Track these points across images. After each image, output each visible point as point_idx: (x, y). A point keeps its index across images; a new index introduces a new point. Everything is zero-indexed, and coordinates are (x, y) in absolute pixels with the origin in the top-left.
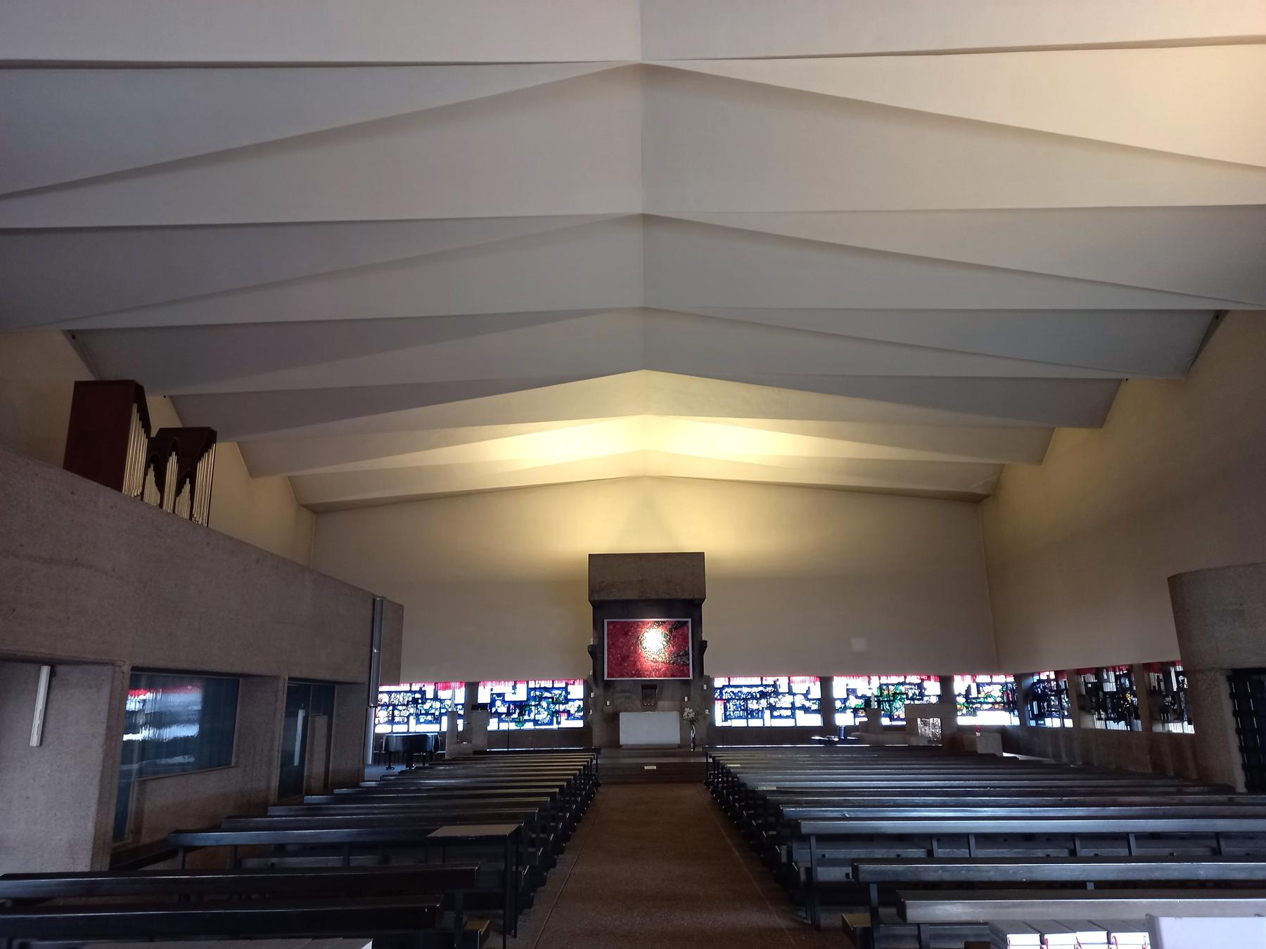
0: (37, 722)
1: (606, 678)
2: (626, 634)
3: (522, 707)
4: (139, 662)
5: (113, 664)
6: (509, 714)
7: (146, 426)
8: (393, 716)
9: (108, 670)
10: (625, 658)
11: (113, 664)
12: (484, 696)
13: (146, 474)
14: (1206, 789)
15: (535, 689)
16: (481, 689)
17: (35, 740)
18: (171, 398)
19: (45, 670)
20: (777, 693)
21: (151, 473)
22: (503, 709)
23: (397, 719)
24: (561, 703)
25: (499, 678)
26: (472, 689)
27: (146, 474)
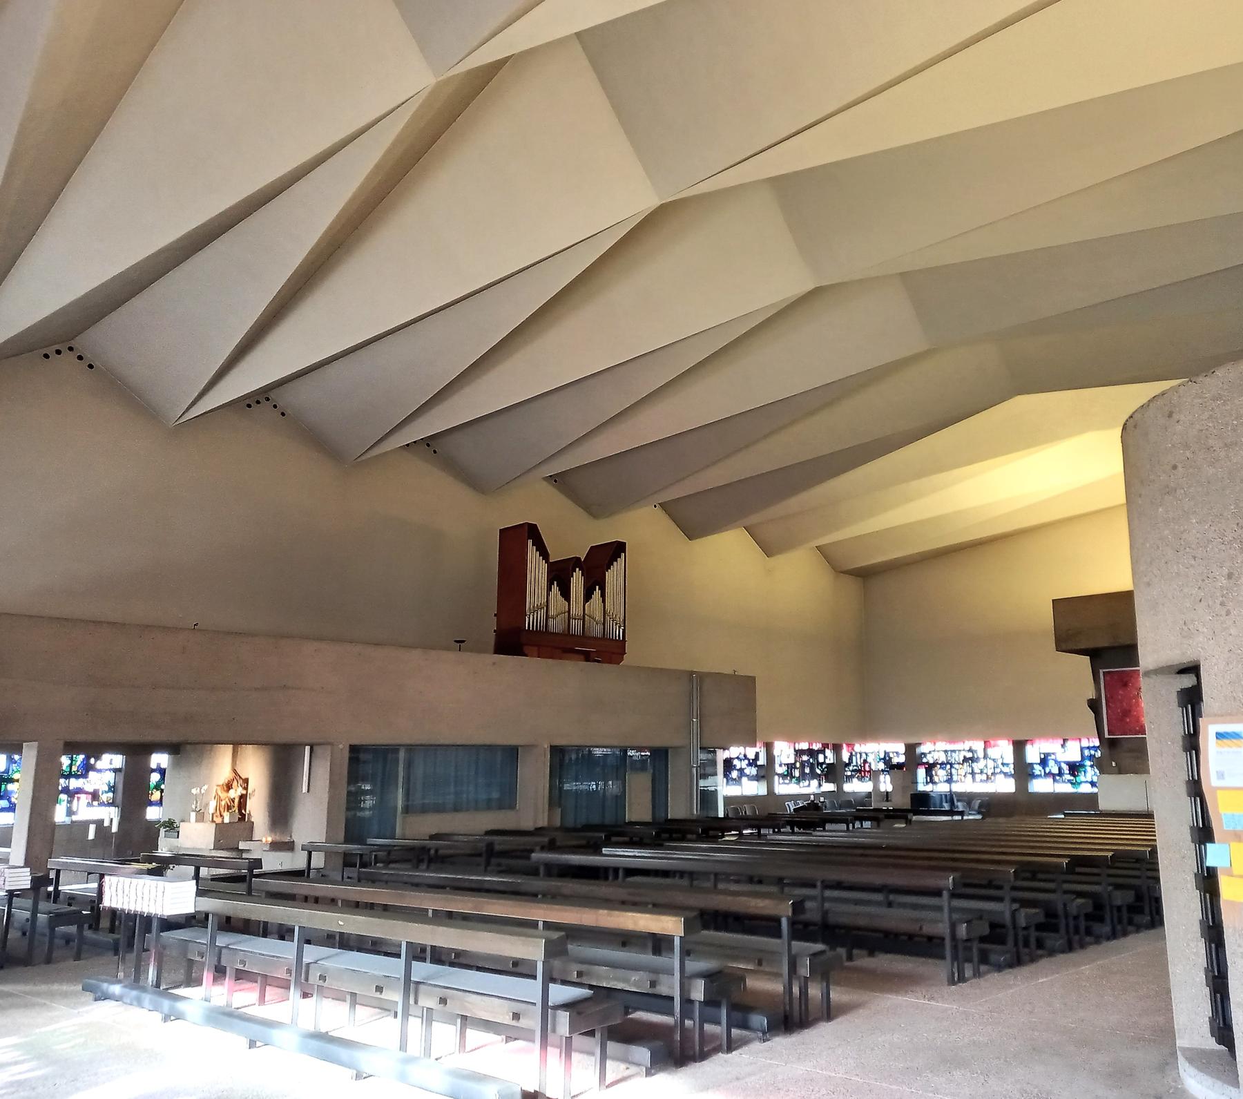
0: (305, 779)
1: (1107, 736)
2: (1125, 685)
3: (1074, 768)
4: (356, 742)
5: (331, 744)
6: (1060, 774)
7: (544, 554)
8: (951, 774)
9: (329, 747)
10: (1127, 713)
11: (331, 744)
12: (1032, 754)
13: (549, 589)
14: (456, 838)
15: (1088, 748)
16: (1029, 748)
17: (305, 789)
18: (663, 506)
19: (307, 749)
20: (973, 760)
21: (555, 588)
22: (1055, 771)
23: (955, 778)
24: (77, 777)
25: (1047, 735)
26: (1019, 747)
27: (549, 589)
